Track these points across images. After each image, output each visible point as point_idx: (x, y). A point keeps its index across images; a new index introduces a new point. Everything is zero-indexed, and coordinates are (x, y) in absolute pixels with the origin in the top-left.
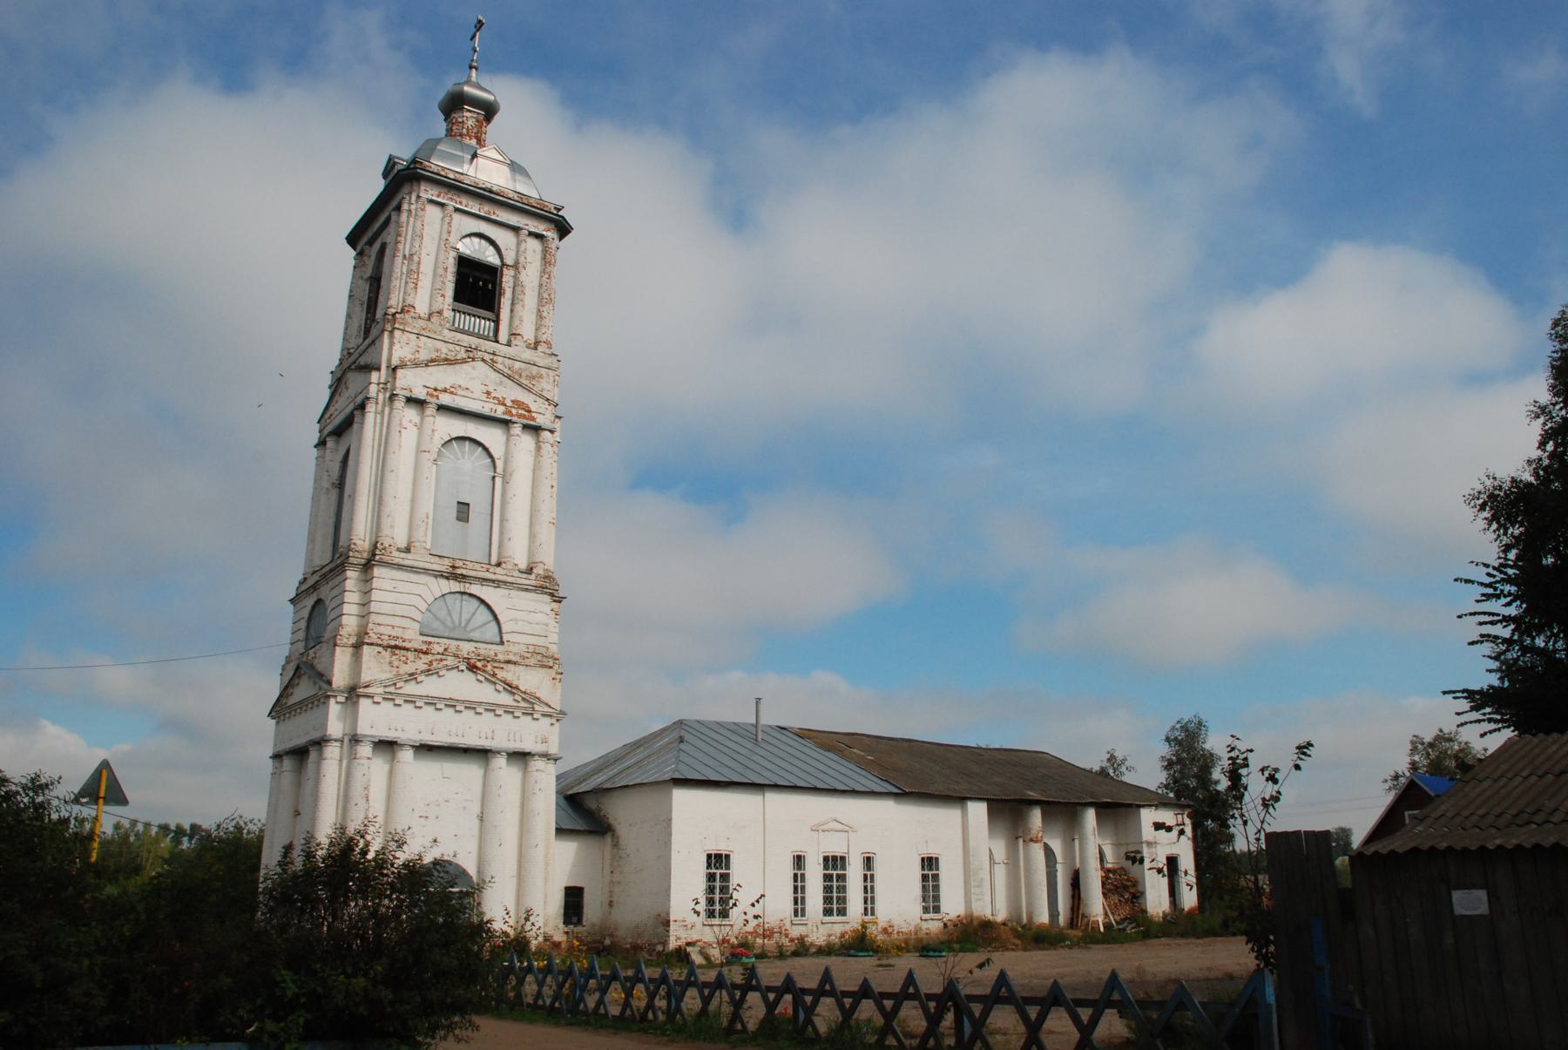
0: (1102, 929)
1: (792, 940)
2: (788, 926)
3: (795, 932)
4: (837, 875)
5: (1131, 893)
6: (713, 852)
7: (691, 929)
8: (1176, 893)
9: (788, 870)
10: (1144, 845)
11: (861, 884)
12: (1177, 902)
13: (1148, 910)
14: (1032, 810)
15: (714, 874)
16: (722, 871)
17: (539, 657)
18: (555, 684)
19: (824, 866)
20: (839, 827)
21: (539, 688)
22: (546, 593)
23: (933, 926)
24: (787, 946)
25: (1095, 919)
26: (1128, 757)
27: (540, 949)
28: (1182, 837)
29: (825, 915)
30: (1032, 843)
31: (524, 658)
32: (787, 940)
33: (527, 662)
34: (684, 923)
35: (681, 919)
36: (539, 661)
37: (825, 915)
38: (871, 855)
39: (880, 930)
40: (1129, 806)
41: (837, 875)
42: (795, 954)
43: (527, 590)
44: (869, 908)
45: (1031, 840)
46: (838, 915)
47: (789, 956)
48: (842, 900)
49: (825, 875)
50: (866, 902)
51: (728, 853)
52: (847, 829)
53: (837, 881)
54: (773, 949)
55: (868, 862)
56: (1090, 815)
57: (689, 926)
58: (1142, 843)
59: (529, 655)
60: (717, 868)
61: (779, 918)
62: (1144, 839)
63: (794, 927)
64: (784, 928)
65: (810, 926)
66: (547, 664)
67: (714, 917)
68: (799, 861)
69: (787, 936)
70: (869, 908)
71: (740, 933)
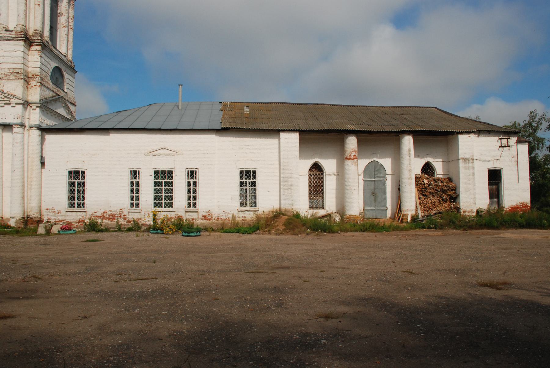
0: (409, 219)
1: (129, 222)
2: (126, 213)
3: (131, 217)
4: (165, 182)
5: (448, 195)
6: (73, 170)
7: (58, 213)
8: (500, 196)
9: (127, 178)
10: (461, 161)
11: (185, 188)
12: (500, 202)
13: (461, 207)
14: (347, 138)
15: (74, 182)
16: (79, 181)
17: (15, 74)
18: (36, 88)
19: (155, 177)
20: (168, 152)
21: (15, 90)
22: (20, 40)
23: (249, 216)
24: (125, 225)
25: (406, 213)
26: (546, 114)
27: (91, 223)
28: (20, 107)
29: (241, 206)
30: (346, 161)
31: (6, 75)
32: (125, 221)
33: (8, 77)
34: (53, 211)
35: (51, 208)
36: (15, 76)
37: (241, 206)
38: (195, 170)
39: (200, 216)
40: (452, 133)
41: (165, 182)
42: (130, 230)
43: (8, 40)
44: (192, 201)
45: (346, 158)
46: (165, 207)
47: (124, 231)
48: (170, 198)
49: (155, 182)
50: (132, 199)
51: (83, 170)
52: (173, 153)
53: (165, 186)
54: (114, 226)
55: (192, 174)
56: (408, 141)
57: (57, 212)
58: (459, 159)
59: (9, 74)
60: (76, 179)
61: (119, 208)
62: (461, 155)
63: (130, 214)
64: (123, 214)
65: (143, 213)
66: (20, 77)
67: (74, 207)
68: (135, 174)
69: (125, 219)
70: (192, 201)
71: (91, 216)
